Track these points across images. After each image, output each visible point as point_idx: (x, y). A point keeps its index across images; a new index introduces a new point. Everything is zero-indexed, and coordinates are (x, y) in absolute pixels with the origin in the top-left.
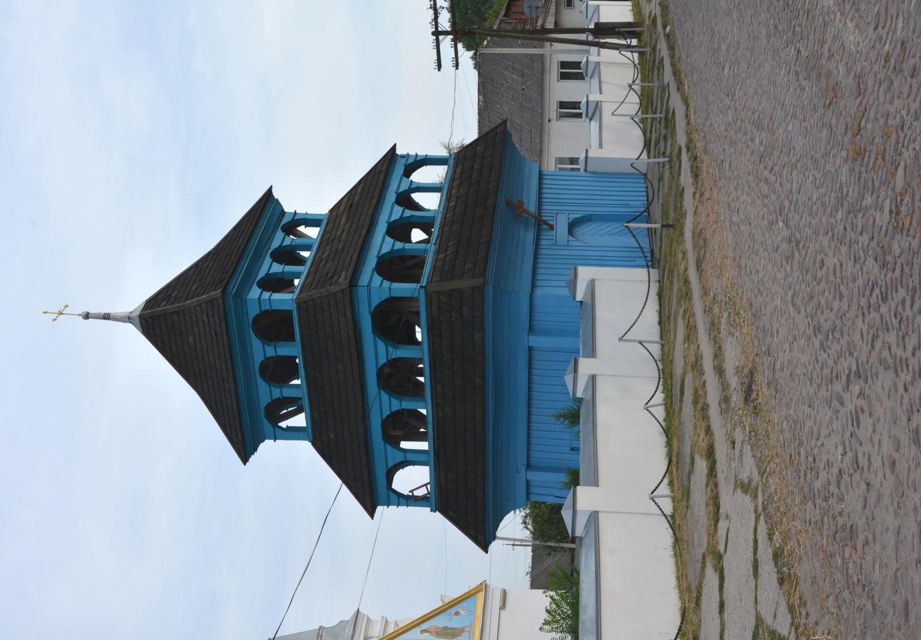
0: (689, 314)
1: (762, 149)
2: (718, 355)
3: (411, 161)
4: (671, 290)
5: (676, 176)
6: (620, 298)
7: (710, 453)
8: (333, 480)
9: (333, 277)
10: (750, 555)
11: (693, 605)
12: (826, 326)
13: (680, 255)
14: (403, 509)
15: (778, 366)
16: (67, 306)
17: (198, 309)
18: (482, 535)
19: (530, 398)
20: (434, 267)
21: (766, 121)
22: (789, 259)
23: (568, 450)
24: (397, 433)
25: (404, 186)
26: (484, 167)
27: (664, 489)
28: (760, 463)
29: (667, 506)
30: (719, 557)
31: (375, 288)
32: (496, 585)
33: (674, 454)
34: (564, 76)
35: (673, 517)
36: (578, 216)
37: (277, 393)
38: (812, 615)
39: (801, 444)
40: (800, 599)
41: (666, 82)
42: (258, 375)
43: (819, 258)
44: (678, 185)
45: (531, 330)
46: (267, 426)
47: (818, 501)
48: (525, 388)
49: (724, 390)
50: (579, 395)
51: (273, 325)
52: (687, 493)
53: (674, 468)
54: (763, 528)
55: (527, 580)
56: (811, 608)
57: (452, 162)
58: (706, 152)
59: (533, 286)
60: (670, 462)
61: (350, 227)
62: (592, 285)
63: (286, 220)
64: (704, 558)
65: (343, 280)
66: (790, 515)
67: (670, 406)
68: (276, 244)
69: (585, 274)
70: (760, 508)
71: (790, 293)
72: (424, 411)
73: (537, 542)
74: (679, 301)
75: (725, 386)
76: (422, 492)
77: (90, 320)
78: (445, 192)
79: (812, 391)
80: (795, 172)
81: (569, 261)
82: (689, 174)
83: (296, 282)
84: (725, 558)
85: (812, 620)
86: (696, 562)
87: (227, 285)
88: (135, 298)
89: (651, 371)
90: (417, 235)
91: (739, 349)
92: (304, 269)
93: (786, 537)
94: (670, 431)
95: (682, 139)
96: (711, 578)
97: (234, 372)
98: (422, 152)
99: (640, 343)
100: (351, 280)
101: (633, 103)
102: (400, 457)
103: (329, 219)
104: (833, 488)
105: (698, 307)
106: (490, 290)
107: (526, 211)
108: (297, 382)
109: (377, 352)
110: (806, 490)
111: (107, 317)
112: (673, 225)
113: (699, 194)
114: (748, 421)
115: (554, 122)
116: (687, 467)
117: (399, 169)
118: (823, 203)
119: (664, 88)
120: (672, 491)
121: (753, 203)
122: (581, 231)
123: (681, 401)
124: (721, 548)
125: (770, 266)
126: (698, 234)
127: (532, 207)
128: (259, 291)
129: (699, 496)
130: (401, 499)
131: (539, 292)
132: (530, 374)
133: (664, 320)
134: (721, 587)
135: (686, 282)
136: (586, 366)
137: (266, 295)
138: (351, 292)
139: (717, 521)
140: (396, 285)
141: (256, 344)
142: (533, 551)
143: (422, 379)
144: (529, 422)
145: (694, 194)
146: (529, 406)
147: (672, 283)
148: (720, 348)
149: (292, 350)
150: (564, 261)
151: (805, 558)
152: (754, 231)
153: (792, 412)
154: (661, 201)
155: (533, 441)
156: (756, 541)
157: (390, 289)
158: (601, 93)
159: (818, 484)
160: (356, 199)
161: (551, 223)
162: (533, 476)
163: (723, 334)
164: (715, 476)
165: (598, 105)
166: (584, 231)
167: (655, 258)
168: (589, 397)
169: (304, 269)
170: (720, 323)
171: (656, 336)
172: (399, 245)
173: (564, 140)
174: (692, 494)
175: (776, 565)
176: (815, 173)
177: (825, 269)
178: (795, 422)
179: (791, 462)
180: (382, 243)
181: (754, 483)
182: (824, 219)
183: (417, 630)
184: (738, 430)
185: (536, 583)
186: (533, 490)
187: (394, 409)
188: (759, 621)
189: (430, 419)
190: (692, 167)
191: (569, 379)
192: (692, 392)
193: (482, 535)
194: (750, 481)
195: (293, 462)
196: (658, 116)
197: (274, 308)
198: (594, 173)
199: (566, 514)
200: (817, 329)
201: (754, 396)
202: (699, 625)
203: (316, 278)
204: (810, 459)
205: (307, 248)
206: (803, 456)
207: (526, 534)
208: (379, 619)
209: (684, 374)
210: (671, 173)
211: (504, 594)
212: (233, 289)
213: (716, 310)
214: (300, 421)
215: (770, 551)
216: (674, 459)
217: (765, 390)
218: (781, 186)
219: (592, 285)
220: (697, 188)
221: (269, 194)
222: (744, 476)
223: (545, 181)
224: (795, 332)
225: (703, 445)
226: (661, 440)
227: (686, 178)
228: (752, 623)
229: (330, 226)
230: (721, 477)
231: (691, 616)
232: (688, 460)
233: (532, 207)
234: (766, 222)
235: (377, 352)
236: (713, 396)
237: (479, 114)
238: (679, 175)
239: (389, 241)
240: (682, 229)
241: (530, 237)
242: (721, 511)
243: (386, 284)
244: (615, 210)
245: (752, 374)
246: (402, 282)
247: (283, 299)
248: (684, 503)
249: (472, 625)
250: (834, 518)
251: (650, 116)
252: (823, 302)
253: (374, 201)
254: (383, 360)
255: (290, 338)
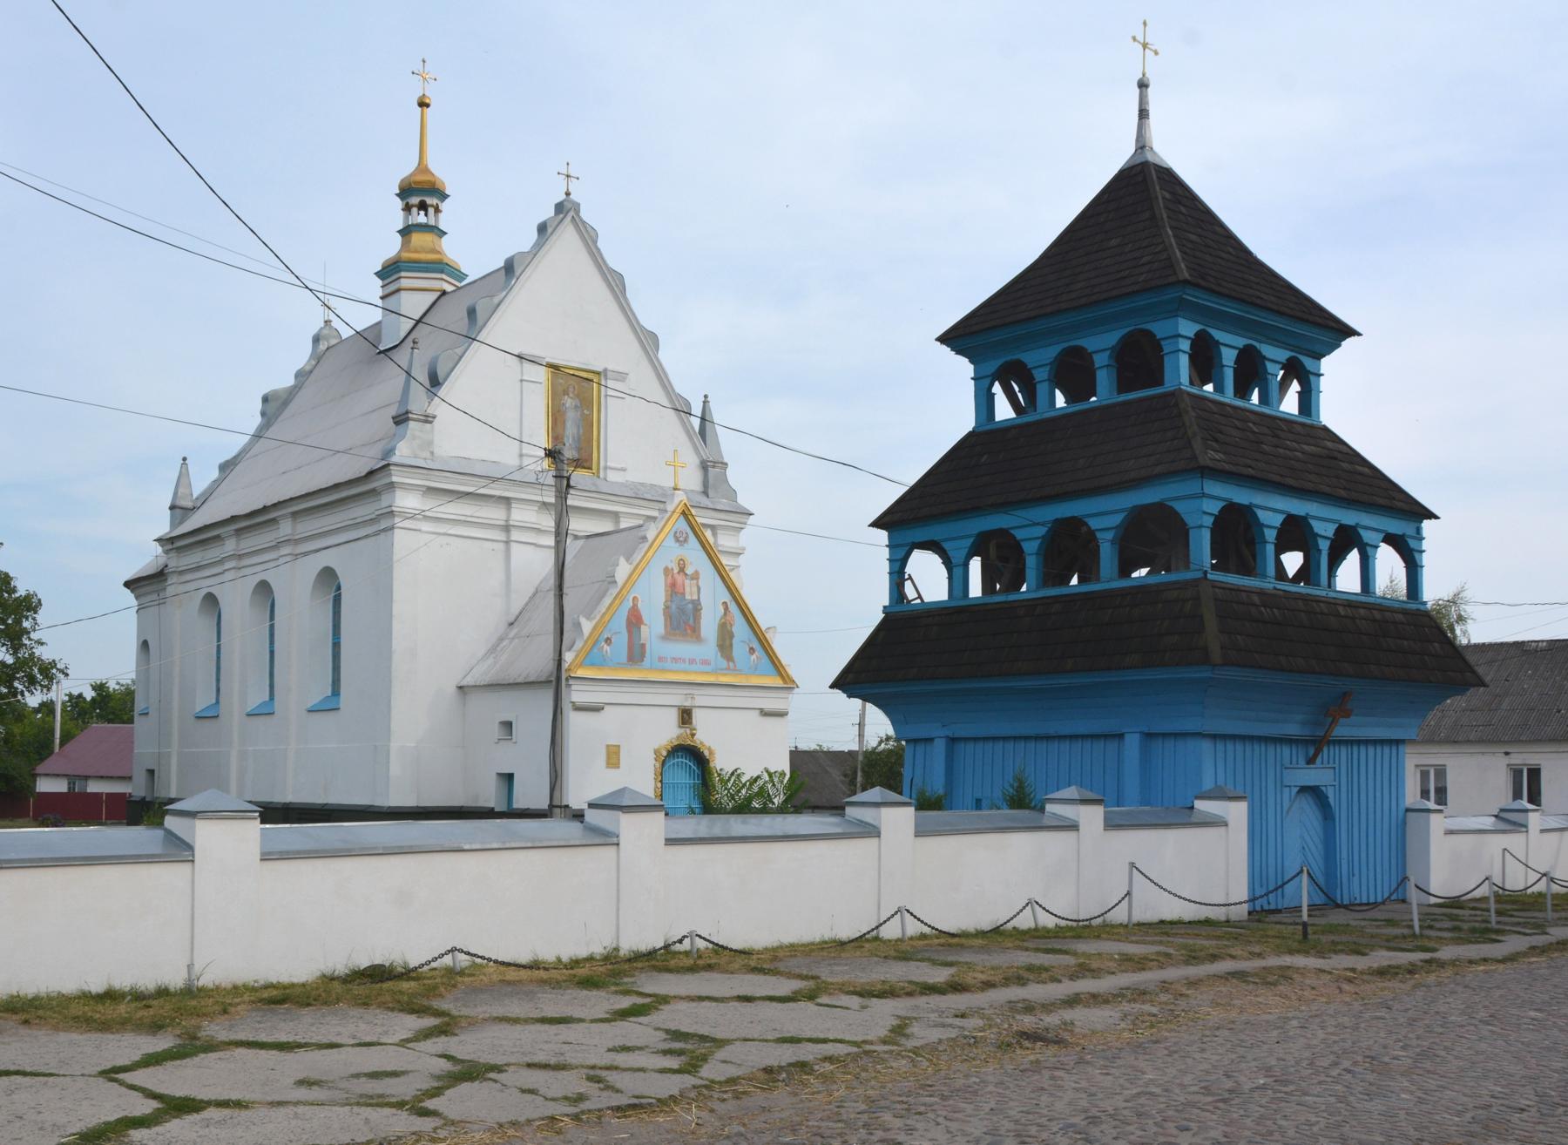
0: (1164, 960)
1: (1386, 1059)
2: (1096, 999)
3: (1412, 543)
4: (1208, 937)
5: (1392, 944)
6: (1200, 864)
7: (956, 987)
8: (913, 474)
9: (1216, 441)
10: (808, 1035)
11: (753, 964)
12: (1095, 1131)
13: (1257, 949)
14: (886, 567)
15: (1057, 1073)
16: (1156, 53)
17: (1160, 248)
18: (852, 680)
19: (1048, 738)
20: (1237, 590)
21: (1428, 1065)
22: (1207, 1091)
23: (978, 795)
24: (993, 552)
25: (1367, 536)
26: (1416, 657)
27: (913, 928)
28: (932, 1049)
29: (891, 932)
30: (811, 996)
31: (1201, 505)
32: (793, 703)
33: (963, 941)
34: (1516, 773)
35: (877, 938)
36: (1331, 800)
37: (1041, 375)
38: (723, 1105)
39: (944, 1098)
40: (744, 1093)
41: (1551, 930)
42: (1065, 345)
43: (1192, 1125)
44: (1373, 948)
45: (1149, 736)
46: (993, 366)
47: (865, 1116)
48: (1052, 732)
49: (1043, 1006)
50: (1049, 807)
51: (1139, 359)
52: (904, 957)
53: (942, 941)
54: (841, 1050)
55: (807, 745)
56: (731, 1105)
57: (1413, 606)
58: (1415, 987)
59: (1214, 737)
60: (953, 935)
61: (1298, 460)
62: (1219, 822)
63: (1307, 362)
64: (813, 978)
65: (1211, 456)
66: (855, 1083)
67: (1036, 935)
68: (1268, 350)
69: (1237, 813)
70: (868, 1047)
71: (1157, 1091)
72: (1024, 588)
73: (860, 758)
74: (1185, 947)
75: (1048, 1007)
76: (910, 592)
77: (1137, 91)
78: (1363, 599)
79: (1012, 1113)
80: (1333, 1100)
81: (1257, 789)
82: (1385, 963)
83: (1209, 388)
84: (810, 1006)
85: (716, 1105)
86: (807, 969)
87: (1197, 286)
88: (1171, 152)
89: (1087, 909)
90: (1293, 561)
91: (1099, 1027)
92: (1229, 397)
93: (825, 1078)
94: (997, 935)
95: (1447, 953)
96: (785, 987)
97: (1067, 310)
98: (1426, 560)
99: (1128, 894)
100: (1211, 469)
101: (1517, 880)
102: (957, 557)
103: (1312, 427)
104: (879, 1134)
105: (1172, 973)
106: (1204, 673)
107: (1333, 723)
108: (1060, 400)
109: (1105, 515)
110: (883, 1103)
111: (1143, 114)
112: (1305, 941)
113: (1353, 976)
114: (991, 1035)
115: (1505, 761)
116: (942, 958)
117: (1396, 526)
118: (1271, 1133)
119: (1541, 928)
120: (911, 938)
121: (1309, 1047)
122: (1308, 807)
123: (1037, 950)
124: (824, 999)
125: (1205, 1066)
126: (1285, 974)
127: (1341, 731)
128: (1192, 335)
129: (897, 972)
130: (898, 564)
131: (1206, 745)
132: (1083, 737)
133: (1164, 928)
134: (771, 999)
135: (1214, 958)
136: (1091, 817)
137: (1185, 345)
138: (1192, 470)
139: (860, 995)
140: (1206, 536)
141: (1112, 338)
142: (850, 753)
143: (1074, 581)
144: (1015, 738)
145: (1353, 970)
146: (1037, 738)
147: (1218, 938)
148: (1106, 1002)
149: (1104, 393)
150: (1257, 782)
151: (795, 1100)
152: (1265, 1047)
153: (991, 1088)
154: (1353, 923)
155: (989, 745)
156: (825, 1041)
157: (1201, 526)
158: (1542, 831)
159: (887, 1117)
160: (1345, 465)
161: (1319, 760)
162: (939, 747)
163: (1126, 1007)
164: (922, 994)
165: (1521, 827)
166: (1308, 811)
167: (1265, 916)
168: (1047, 821)
169: (1229, 397)
170: (1143, 1003)
171: (1138, 916)
172: (1271, 535)
173: (1479, 776)
174: (902, 963)
175: (790, 1065)
176: (1322, 1125)
177: (1175, 1132)
178: (975, 1093)
179: (923, 1087)
180: (1272, 510)
181: (903, 1041)
182: (1248, 1133)
183: (727, 598)
184: (980, 1023)
185: (798, 758)
186: (920, 748)
187: (1098, 535)
188: (721, 1043)
189: (1012, 597)
190: (1398, 967)
191: (1071, 792)
192: (1046, 964)
193: (852, 680)
194: (907, 1036)
195: (944, 406)
196: (1493, 918)
197: (1166, 359)
198: (1404, 823)
199: (875, 793)
200: (1094, 1121)
201: (1027, 1044)
202: (726, 972)
203: (1214, 415)
204: (922, 1109)
205: (1264, 399)
206: (928, 1099)
207: (872, 742)
208: (741, 544)
209: (1075, 954)
210: (1396, 937)
211: (781, 714)
212: (1191, 296)
213: (1164, 997)
214: (1004, 411)
215: (810, 1058)
216: (956, 940)
217: (1032, 1058)
218: (1320, 1083)
219: (1219, 822)
220: (1362, 973)
221: (1347, 332)
222: (915, 1029)
223: (1387, 750)
224: (1100, 1096)
225: (969, 979)
226: (986, 925)
227: (1381, 958)
228: (719, 1036)
229: (1299, 429)
230: (922, 1001)
231: (740, 961)
232: (950, 959)
233: (1341, 731)
234: (1274, 1062)
235: (1105, 515)
236: (1036, 992)
237: (1516, 644)
238: (1389, 949)
239: (1277, 520)
240: (1298, 952)
241: (1292, 729)
242: (874, 1000)
243: (1209, 521)
244: (1344, 855)
245: (1059, 1042)
246: (1212, 543)
247: (1180, 371)
248: (892, 953)
249: (735, 671)
250: (840, 1135)
251: (1493, 906)
252: (1131, 1128)
253: (1343, 493)
254: (1094, 524)
255: (1123, 386)
